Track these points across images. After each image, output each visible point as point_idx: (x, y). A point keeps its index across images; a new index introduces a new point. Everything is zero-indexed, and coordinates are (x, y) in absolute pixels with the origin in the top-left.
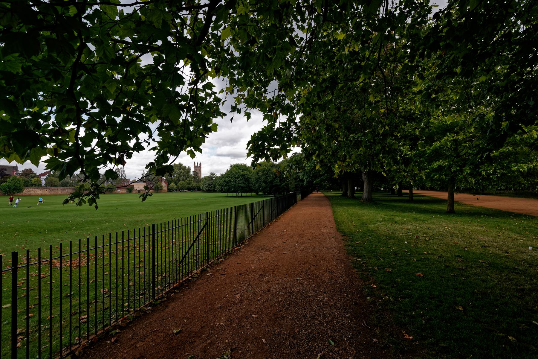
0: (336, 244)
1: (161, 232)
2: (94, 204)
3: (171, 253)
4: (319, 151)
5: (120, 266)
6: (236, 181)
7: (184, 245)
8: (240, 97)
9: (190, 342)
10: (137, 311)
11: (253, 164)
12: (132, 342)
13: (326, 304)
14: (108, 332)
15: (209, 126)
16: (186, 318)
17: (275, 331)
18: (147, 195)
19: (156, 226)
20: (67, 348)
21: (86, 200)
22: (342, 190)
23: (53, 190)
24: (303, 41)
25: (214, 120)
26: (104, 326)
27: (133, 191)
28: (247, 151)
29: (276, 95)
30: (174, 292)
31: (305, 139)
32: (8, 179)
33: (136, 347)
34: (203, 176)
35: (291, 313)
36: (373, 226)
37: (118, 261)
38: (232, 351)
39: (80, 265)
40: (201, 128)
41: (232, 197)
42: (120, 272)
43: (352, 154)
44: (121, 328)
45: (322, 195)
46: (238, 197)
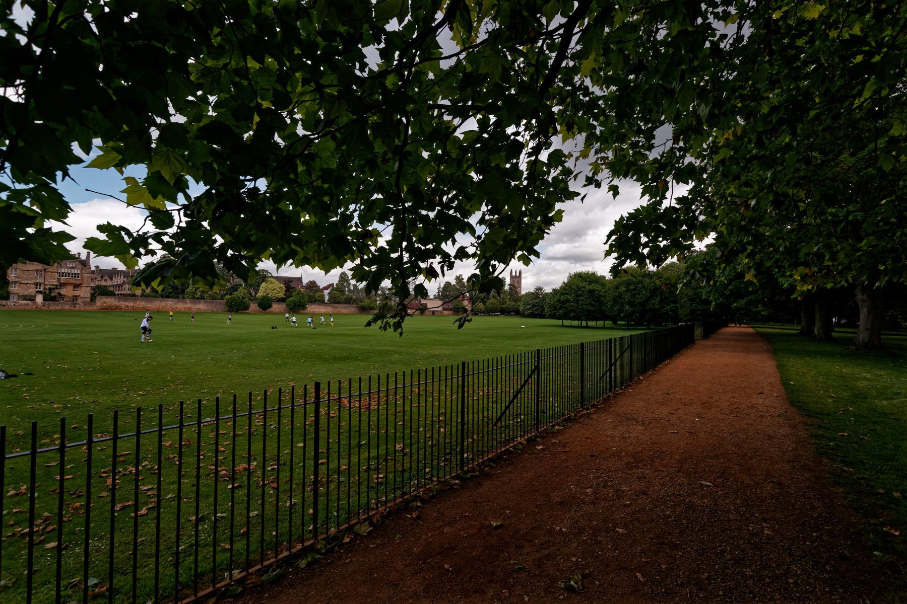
0: (788, 430)
1: (473, 374)
2: (399, 330)
3: (481, 406)
4: (756, 247)
5: (415, 417)
6: (578, 301)
7: (499, 398)
8: (599, 162)
9: (516, 546)
10: (442, 482)
11: (615, 270)
12: (438, 524)
13: (768, 543)
14: (407, 503)
15: (550, 215)
16: (508, 508)
17: (659, 565)
18: (465, 321)
19: (324, 386)
20: (364, 511)
21: (392, 323)
22: (799, 323)
23: (336, 308)
24: (725, 41)
25: (558, 206)
26: (404, 494)
27: (426, 312)
28: (607, 247)
29: (668, 148)
30: (489, 465)
31: (724, 224)
32: (294, 293)
33: (443, 532)
34: (523, 292)
35: (691, 541)
36: (885, 402)
37: (413, 408)
38: (584, 576)
39: (369, 407)
40: (539, 219)
41: (571, 327)
42: (415, 426)
43: (837, 252)
44: (422, 501)
45: (751, 330)
46: (581, 327)
